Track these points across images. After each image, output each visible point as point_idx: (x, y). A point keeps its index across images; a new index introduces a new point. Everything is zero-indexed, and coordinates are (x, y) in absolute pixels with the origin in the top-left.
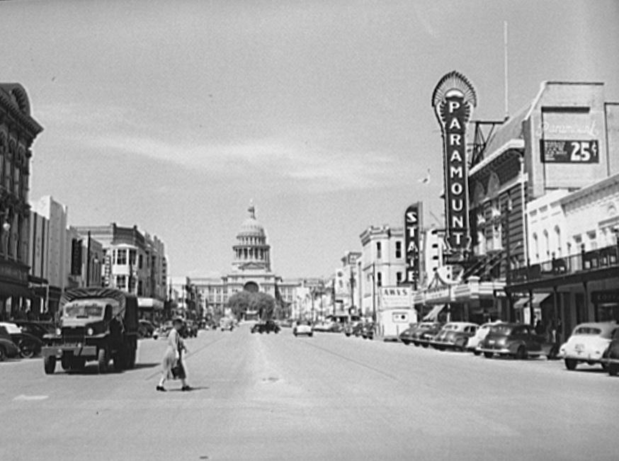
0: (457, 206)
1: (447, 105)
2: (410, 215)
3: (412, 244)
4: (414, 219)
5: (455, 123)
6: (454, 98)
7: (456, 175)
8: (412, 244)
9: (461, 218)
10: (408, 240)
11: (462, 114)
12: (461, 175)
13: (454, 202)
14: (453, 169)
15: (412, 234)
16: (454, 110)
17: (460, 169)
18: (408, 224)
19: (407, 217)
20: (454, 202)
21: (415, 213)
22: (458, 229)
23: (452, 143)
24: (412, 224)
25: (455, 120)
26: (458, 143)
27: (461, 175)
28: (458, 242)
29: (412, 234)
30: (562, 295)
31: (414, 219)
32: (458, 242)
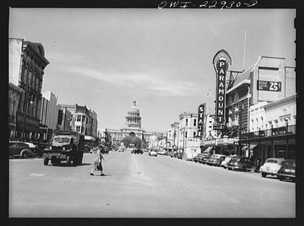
0: (221, 106)
1: (219, 64)
2: (201, 108)
3: (201, 120)
4: (202, 110)
5: (222, 71)
6: (222, 61)
7: (221, 93)
8: (201, 120)
9: (222, 111)
10: (199, 119)
11: (225, 67)
12: (223, 93)
13: (219, 104)
14: (220, 90)
15: (201, 116)
16: (222, 66)
17: (223, 91)
18: (200, 112)
19: (199, 109)
20: (219, 104)
21: (203, 108)
22: (220, 116)
23: (220, 79)
24: (201, 112)
25: (222, 70)
26: (223, 80)
27: (223, 93)
28: (220, 121)
29: (201, 116)
30: (262, 146)
31: (202, 110)
32: (220, 121)
